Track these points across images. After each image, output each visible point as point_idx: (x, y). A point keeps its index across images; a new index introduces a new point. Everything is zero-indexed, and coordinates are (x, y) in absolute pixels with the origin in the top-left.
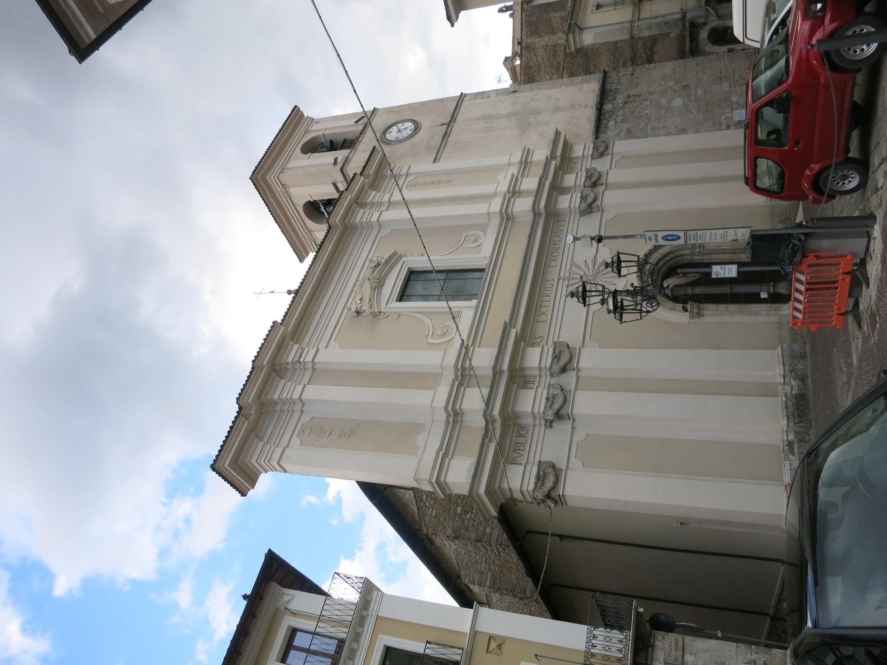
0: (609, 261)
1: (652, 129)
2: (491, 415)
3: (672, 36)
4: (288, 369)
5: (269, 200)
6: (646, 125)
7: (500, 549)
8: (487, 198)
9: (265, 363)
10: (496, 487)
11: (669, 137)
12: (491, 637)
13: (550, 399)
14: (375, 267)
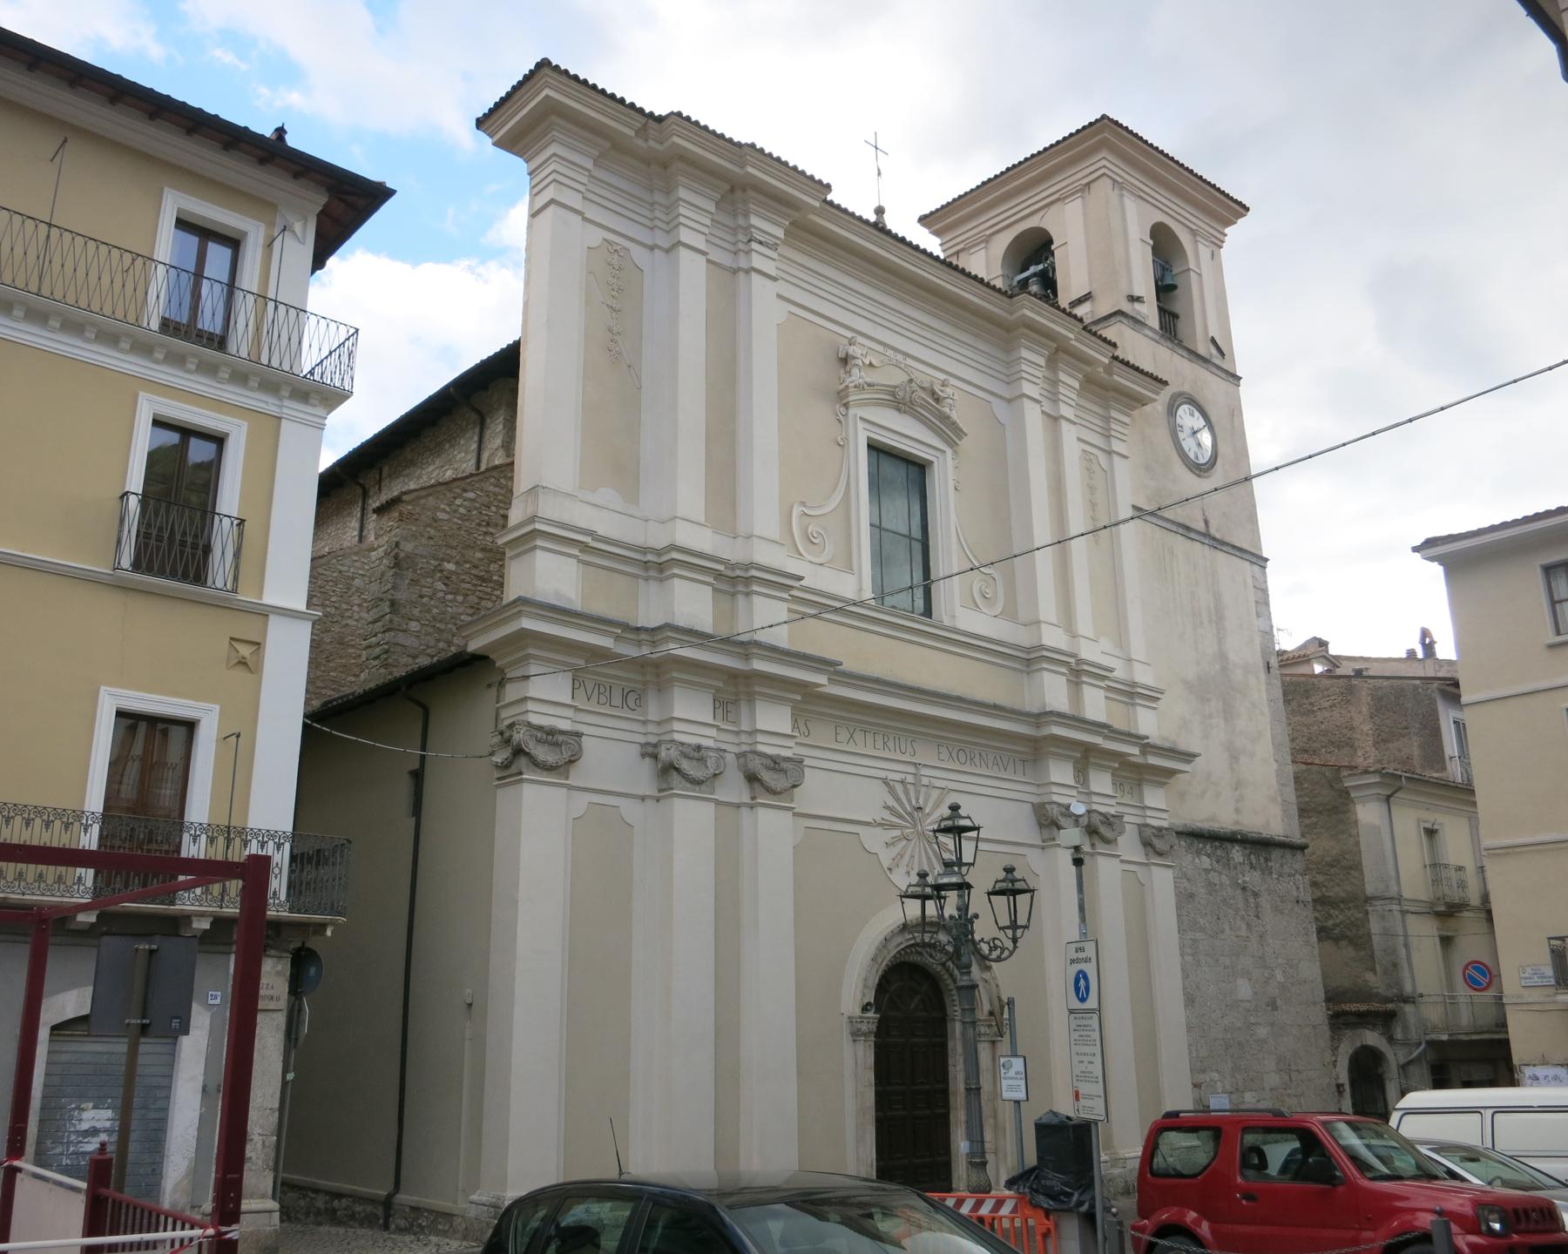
0: (1017, 874)
1: (1194, 941)
2: (667, 640)
3: (1370, 977)
4: (735, 216)
5: (1058, 154)
6: (1202, 930)
7: (377, 650)
8: (1067, 620)
9: (750, 169)
10: (531, 651)
11: (1179, 975)
12: (258, 645)
13: (697, 753)
14: (933, 393)
